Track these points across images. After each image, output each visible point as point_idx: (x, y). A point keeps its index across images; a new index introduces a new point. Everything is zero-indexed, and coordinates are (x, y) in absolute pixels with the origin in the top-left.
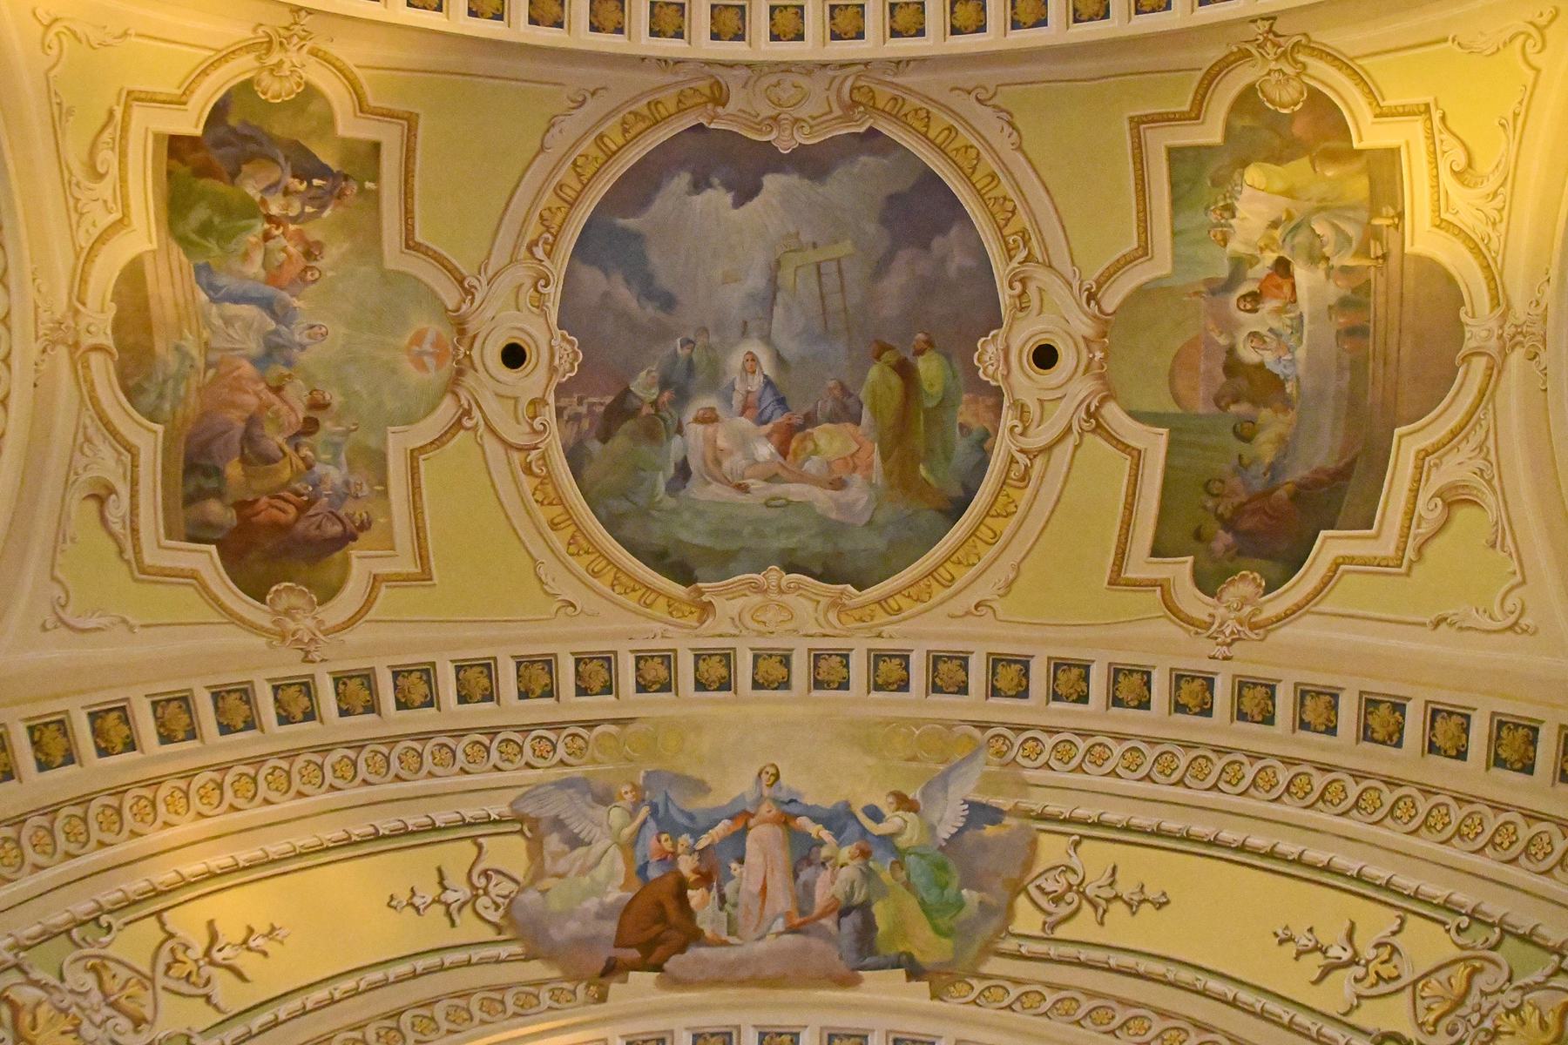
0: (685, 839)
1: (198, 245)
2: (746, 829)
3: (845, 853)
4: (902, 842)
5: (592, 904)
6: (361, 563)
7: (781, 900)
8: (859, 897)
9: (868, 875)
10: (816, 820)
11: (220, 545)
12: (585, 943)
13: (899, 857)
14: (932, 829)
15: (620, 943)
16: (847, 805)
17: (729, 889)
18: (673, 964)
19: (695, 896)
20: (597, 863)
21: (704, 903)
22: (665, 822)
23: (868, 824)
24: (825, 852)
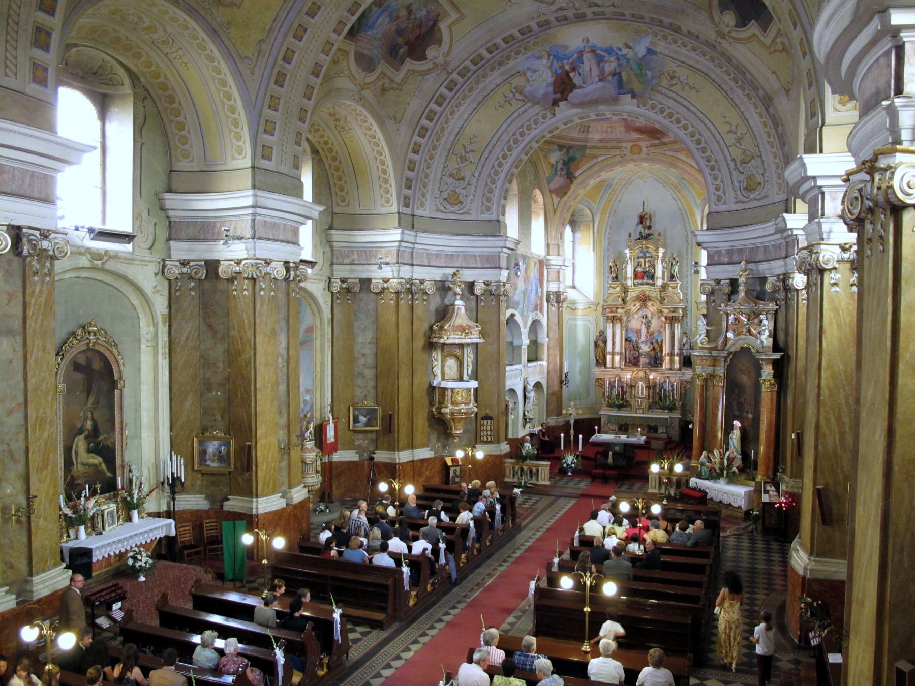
0: (565, 61)
1: (363, 15)
2: (582, 55)
3: (612, 59)
4: (628, 57)
5: (545, 84)
6: (443, 26)
7: (595, 72)
8: (618, 71)
9: (620, 65)
10: (602, 51)
11: (408, 56)
12: (546, 95)
13: (628, 60)
14: (637, 54)
15: (555, 93)
16: (611, 47)
17: (581, 71)
18: (570, 96)
19: (572, 75)
20: (543, 74)
21: (574, 76)
22: (558, 58)
23: (618, 52)
24: (606, 59)
